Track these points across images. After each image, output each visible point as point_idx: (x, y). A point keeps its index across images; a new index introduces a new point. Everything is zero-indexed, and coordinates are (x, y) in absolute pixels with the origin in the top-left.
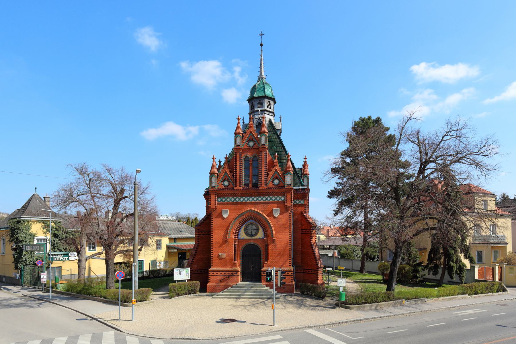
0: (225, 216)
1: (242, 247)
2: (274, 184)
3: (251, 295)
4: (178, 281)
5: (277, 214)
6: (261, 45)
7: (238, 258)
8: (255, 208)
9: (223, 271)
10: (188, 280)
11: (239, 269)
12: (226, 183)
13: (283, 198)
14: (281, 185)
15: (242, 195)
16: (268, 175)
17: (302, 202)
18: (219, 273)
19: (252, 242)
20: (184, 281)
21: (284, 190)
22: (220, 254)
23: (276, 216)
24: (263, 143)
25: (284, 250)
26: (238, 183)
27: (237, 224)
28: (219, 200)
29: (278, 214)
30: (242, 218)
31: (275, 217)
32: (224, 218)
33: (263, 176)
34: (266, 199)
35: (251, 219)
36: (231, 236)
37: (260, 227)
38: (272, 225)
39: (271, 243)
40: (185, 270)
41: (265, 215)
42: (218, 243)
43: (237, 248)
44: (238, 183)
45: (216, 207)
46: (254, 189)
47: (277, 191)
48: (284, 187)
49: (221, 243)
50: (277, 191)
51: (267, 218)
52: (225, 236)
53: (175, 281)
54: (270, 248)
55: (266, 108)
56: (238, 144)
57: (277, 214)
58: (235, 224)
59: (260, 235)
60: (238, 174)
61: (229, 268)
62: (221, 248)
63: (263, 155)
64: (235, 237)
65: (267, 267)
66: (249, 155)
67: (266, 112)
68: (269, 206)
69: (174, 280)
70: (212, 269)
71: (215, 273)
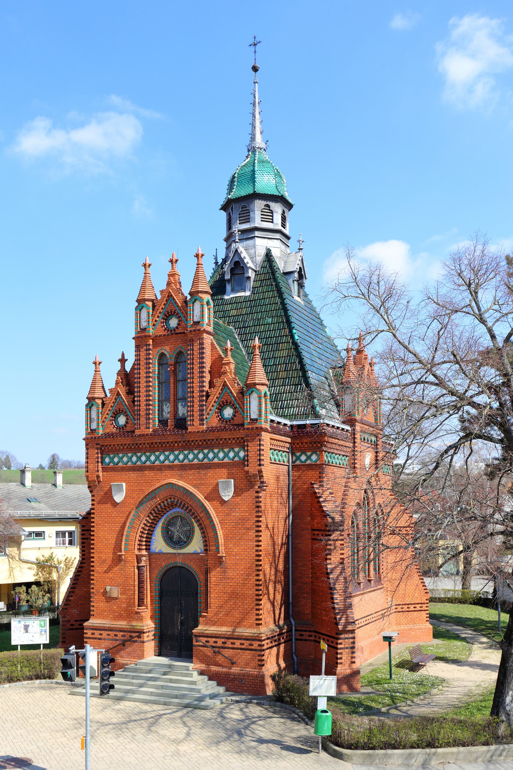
0: (118, 498)
1: (158, 573)
2: (222, 419)
3: (152, 694)
4: (24, 647)
5: (227, 495)
6: (255, 69)
7: (148, 600)
8: (181, 478)
9: (111, 629)
10: (45, 646)
11: (148, 625)
12: (122, 420)
13: (242, 454)
14: (237, 421)
15: (152, 448)
16: (208, 396)
17: (314, 457)
18: (105, 633)
19: (179, 562)
20: (36, 647)
21: (241, 433)
22: (108, 588)
23: (226, 499)
24: (196, 319)
25: (244, 584)
26: (143, 420)
27: (144, 520)
28: (107, 460)
29: (231, 494)
30: (152, 503)
31: (223, 502)
32: (115, 504)
33: (196, 400)
34: (206, 456)
35: (173, 506)
36: (131, 546)
37: (195, 525)
38: (216, 521)
39: (215, 567)
40: (37, 622)
41: (201, 497)
42: (104, 561)
43: (147, 574)
44: (143, 420)
45: (98, 477)
46: (177, 432)
47: (226, 435)
48: (243, 425)
49: (109, 561)
50: (226, 435)
51: (207, 504)
52: (118, 547)
53: (15, 648)
54: (214, 577)
55: (258, 222)
56: (144, 324)
57: (227, 495)
58: (139, 516)
59: (196, 545)
60: (143, 399)
61: (122, 624)
62: (110, 575)
63: (196, 347)
64: (139, 549)
65: (206, 624)
66: (166, 350)
67: (257, 233)
68: (211, 473)
69: (13, 643)
70: (93, 622)
71: (97, 633)
